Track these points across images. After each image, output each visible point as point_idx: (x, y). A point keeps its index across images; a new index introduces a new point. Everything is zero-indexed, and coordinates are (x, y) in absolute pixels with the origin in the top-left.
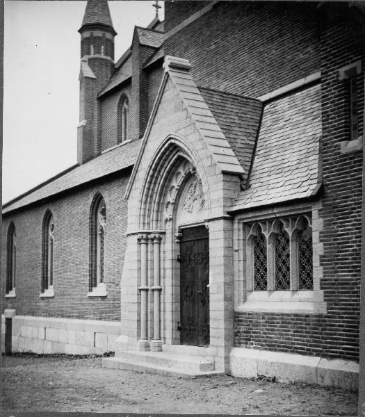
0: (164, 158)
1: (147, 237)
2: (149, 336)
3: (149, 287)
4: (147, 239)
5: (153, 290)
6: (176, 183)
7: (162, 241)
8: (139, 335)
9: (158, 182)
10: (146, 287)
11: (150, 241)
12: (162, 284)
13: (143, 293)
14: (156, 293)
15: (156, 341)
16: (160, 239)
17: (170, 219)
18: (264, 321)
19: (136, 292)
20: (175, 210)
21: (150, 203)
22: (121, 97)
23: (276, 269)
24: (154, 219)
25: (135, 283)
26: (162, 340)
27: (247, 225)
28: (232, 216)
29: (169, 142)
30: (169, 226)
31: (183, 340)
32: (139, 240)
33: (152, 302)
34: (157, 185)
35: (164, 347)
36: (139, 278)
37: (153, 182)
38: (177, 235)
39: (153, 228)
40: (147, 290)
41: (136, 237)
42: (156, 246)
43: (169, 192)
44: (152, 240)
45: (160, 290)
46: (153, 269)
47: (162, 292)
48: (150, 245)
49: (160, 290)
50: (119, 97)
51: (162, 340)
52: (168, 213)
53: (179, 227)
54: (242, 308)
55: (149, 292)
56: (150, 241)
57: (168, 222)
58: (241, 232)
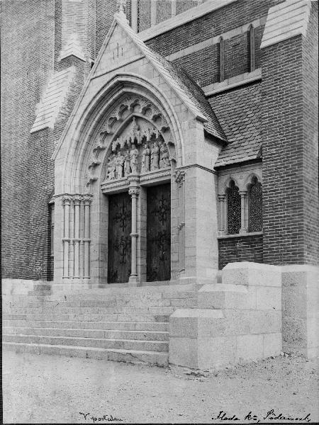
10: (89, 239)
14: (86, 244)
45: (89, 242)
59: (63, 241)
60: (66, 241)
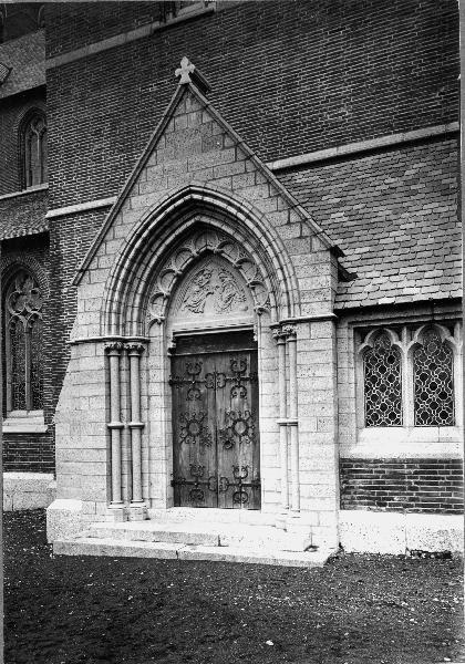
0: (166, 224)
1: (122, 347)
2: (126, 496)
3: (124, 424)
4: (120, 350)
5: (130, 428)
6: (177, 266)
7: (145, 354)
8: (110, 497)
9: (146, 261)
10: (119, 424)
11: (125, 353)
12: (145, 419)
13: (115, 433)
14: (136, 433)
15: (139, 505)
16: (141, 351)
17: (162, 321)
18: (412, 471)
19: (103, 430)
20: (168, 308)
21: (128, 294)
22: (27, 115)
23: (452, 395)
24: (135, 319)
25: (102, 416)
26: (147, 503)
27: (360, 334)
28: (340, 317)
29: (187, 198)
30: (157, 331)
31: (177, 501)
32: (108, 350)
33: (130, 445)
34: (143, 266)
35: (151, 512)
36: (109, 409)
37: (137, 260)
38: (171, 345)
39: (133, 332)
40: (121, 429)
41: (101, 348)
42: (134, 362)
43: (159, 279)
44: (129, 351)
45: (141, 428)
46: (129, 394)
47: (146, 431)
48: (124, 359)
49: (141, 428)
50: (20, 116)
51: (147, 503)
52: (157, 312)
53: (174, 333)
54: (356, 451)
55: (125, 432)
56: (125, 353)
57: (155, 325)
58: (352, 342)
59: (110, 429)
60: (115, 428)
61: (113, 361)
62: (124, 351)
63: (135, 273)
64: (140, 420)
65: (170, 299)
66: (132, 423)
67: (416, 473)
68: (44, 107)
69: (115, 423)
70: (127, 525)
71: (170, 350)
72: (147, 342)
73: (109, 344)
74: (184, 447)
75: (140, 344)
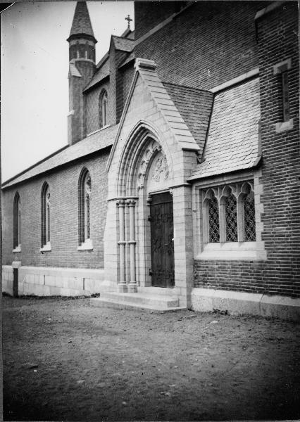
3: (126, 242)
4: (124, 203)
7: (136, 205)
8: (119, 280)
10: (124, 242)
12: (136, 239)
13: (121, 246)
14: (132, 246)
16: (134, 203)
19: (116, 246)
20: (146, 180)
22: (102, 92)
26: (137, 284)
29: (140, 126)
30: (141, 192)
32: (117, 204)
38: (148, 199)
42: (131, 209)
44: (128, 204)
45: (135, 244)
47: (137, 245)
48: (126, 208)
49: (135, 244)
51: (137, 284)
52: (140, 183)
54: (201, 256)
56: (126, 205)
58: (198, 197)
60: (132, 243)
61: (121, 209)
62: (196, 195)
63: (128, 164)
64: (135, 240)
65: (146, 175)
66: (130, 242)
67: (219, 268)
68: (250, 38)
69: (121, 241)
70: (125, 294)
71: (149, 202)
72: (137, 199)
73: (118, 201)
74: (155, 253)
75: (132, 201)
